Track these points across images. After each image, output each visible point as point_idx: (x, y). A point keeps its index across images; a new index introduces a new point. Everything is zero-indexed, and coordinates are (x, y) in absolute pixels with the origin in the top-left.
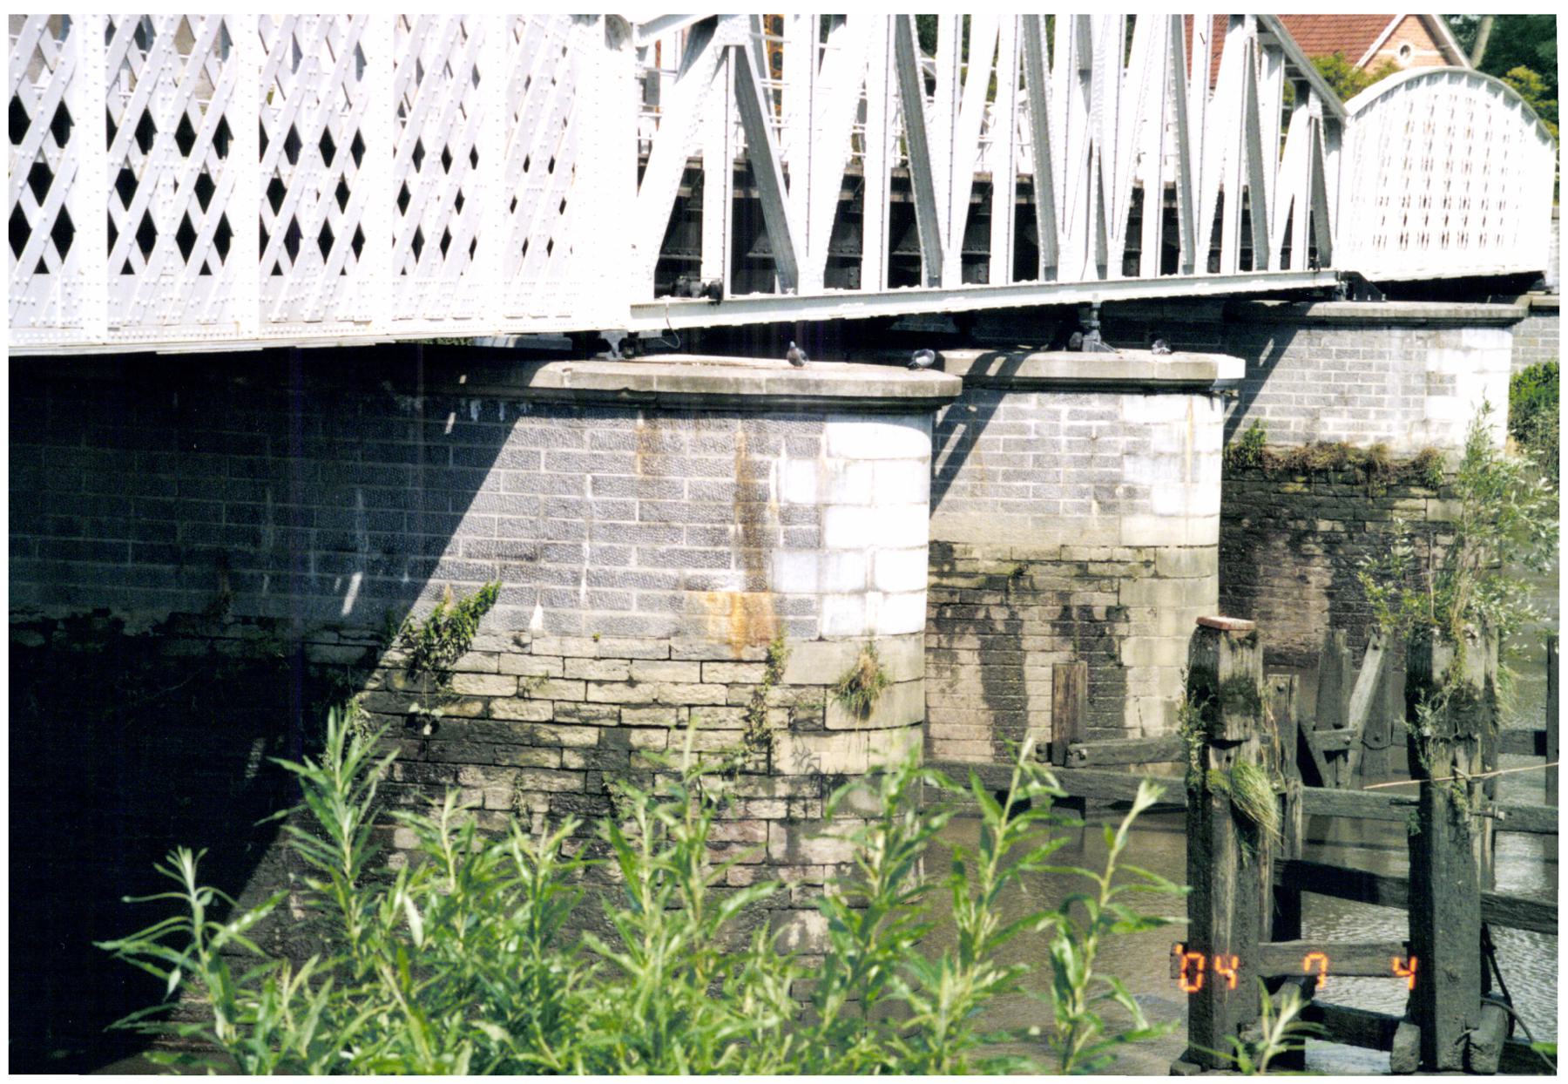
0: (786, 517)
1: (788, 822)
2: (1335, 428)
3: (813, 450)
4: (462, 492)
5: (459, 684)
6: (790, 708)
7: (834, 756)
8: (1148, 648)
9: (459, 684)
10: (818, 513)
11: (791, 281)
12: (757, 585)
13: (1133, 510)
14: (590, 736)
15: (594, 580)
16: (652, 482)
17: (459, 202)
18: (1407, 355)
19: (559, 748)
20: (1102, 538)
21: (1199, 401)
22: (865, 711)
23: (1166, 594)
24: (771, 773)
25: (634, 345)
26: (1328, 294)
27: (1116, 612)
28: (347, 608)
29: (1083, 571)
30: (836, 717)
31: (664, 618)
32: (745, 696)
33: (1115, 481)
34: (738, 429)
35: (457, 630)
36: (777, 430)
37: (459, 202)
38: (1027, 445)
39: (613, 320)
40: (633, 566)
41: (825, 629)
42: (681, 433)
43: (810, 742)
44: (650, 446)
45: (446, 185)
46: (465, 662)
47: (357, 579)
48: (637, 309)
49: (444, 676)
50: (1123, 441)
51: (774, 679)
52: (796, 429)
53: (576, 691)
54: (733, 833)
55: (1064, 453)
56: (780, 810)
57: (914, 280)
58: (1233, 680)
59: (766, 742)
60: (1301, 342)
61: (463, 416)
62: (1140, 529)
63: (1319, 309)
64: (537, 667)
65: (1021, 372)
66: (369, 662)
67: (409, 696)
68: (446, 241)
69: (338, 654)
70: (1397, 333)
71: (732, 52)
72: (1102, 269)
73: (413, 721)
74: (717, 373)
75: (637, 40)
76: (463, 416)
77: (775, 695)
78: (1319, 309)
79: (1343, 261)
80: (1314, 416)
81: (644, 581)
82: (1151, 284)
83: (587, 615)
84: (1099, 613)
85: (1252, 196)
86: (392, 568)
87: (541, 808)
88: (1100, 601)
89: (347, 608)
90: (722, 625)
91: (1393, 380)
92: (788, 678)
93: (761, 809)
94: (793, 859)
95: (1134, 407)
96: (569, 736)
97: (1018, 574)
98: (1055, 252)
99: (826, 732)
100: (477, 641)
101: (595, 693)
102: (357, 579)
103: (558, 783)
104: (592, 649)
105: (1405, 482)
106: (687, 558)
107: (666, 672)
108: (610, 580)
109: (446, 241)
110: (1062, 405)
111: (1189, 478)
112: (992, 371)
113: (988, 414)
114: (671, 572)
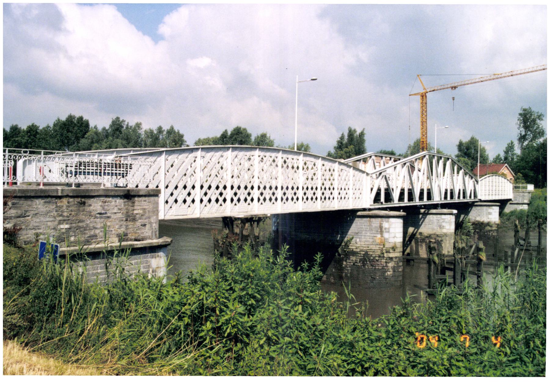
0: (385, 229)
1: (386, 262)
2: (478, 219)
3: (388, 222)
4: (350, 226)
5: (350, 247)
6: (386, 250)
7: (391, 255)
8: (445, 245)
9: (350, 247)
10: (389, 229)
11: (393, 201)
12: (382, 236)
13: (443, 228)
14: (364, 253)
15: (364, 236)
16: (370, 225)
17: (347, 194)
18: (486, 210)
19: (360, 254)
20: (440, 231)
21: (451, 216)
22: (394, 250)
23: (447, 238)
24: (384, 257)
25: (370, 210)
26: (477, 202)
27: (442, 241)
28: (338, 239)
29: (437, 236)
30: (391, 251)
31: (371, 240)
32: (381, 249)
33: (441, 225)
34: (379, 219)
35: (349, 241)
36: (384, 219)
37: (347, 194)
38: (430, 221)
39: (367, 206)
40: (368, 234)
41: (390, 241)
42: (373, 220)
43: (388, 254)
44: (370, 221)
45: (345, 192)
46: (351, 245)
47: (339, 236)
48: (371, 205)
49: (348, 246)
50: (442, 220)
51: (384, 247)
52: (387, 219)
53: (362, 248)
54: (379, 263)
55: (435, 222)
56: (385, 261)
57: (431, 200)
58: (433, 247)
59: (383, 253)
60: (474, 208)
61: (350, 218)
62: (444, 231)
63: (476, 204)
64: (358, 245)
65: (430, 212)
66: (340, 245)
67: (345, 248)
68: (345, 198)
69: (337, 244)
70: (485, 207)
71: (384, 176)
72: (441, 199)
73: (345, 251)
74: (379, 213)
75: (370, 175)
76: (350, 218)
77: (384, 249)
78: (476, 204)
79: (479, 197)
80: (476, 217)
81: (370, 236)
82: (449, 200)
83: (363, 240)
84: (439, 240)
85: (51, 221)
86: (343, 235)
87: (359, 260)
88: (440, 239)
89: (338, 239)
90: (378, 241)
91: (485, 213)
92: (386, 247)
93: (383, 261)
94: (386, 266)
95: (443, 216)
96: (362, 253)
97: (430, 236)
98: (433, 197)
99: (390, 252)
100: (352, 243)
101: (364, 248)
102: (339, 236)
103: (360, 258)
104: (364, 243)
105: (486, 225)
106: (374, 233)
107: (372, 246)
108: (365, 236)
109: (345, 198)
110: (435, 216)
111: (450, 225)
112: (426, 212)
113: (426, 217)
114: (372, 235)
